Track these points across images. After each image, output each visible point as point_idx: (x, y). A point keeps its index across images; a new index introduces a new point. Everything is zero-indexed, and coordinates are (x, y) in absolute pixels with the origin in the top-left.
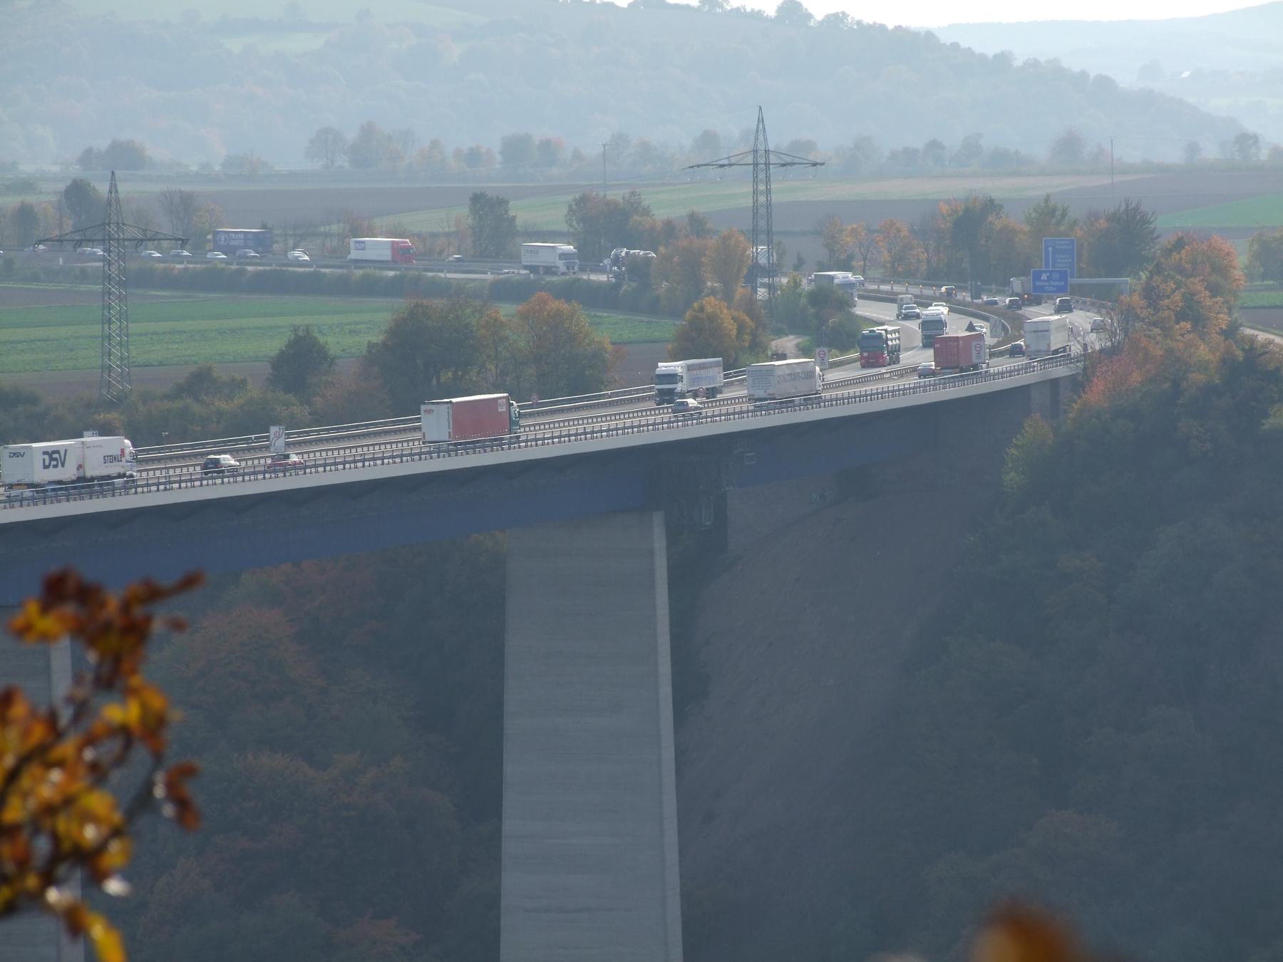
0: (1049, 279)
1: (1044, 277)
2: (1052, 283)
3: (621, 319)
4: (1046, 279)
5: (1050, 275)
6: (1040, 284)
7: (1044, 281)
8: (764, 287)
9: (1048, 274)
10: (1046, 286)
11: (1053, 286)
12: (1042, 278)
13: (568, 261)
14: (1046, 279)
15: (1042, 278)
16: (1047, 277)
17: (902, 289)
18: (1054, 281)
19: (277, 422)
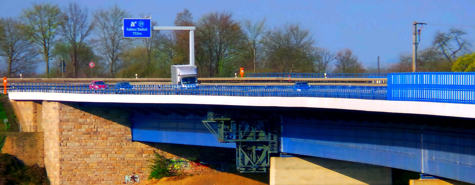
0: (137, 26)
1: (133, 24)
2: (139, 29)
3: (33, 143)
4: (134, 26)
5: (137, 23)
6: (130, 30)
7: (133, 27)
8: (78, 129)
9: (136, 22)
10: (134, 31)
11: (139, 32)
12: (131, 26)
13: (260, 166)
14: (134, 26)
15: (131, 26)
16: (135, 24)
17: (174, 158)
18: (141, 28)
19: (422, 134)
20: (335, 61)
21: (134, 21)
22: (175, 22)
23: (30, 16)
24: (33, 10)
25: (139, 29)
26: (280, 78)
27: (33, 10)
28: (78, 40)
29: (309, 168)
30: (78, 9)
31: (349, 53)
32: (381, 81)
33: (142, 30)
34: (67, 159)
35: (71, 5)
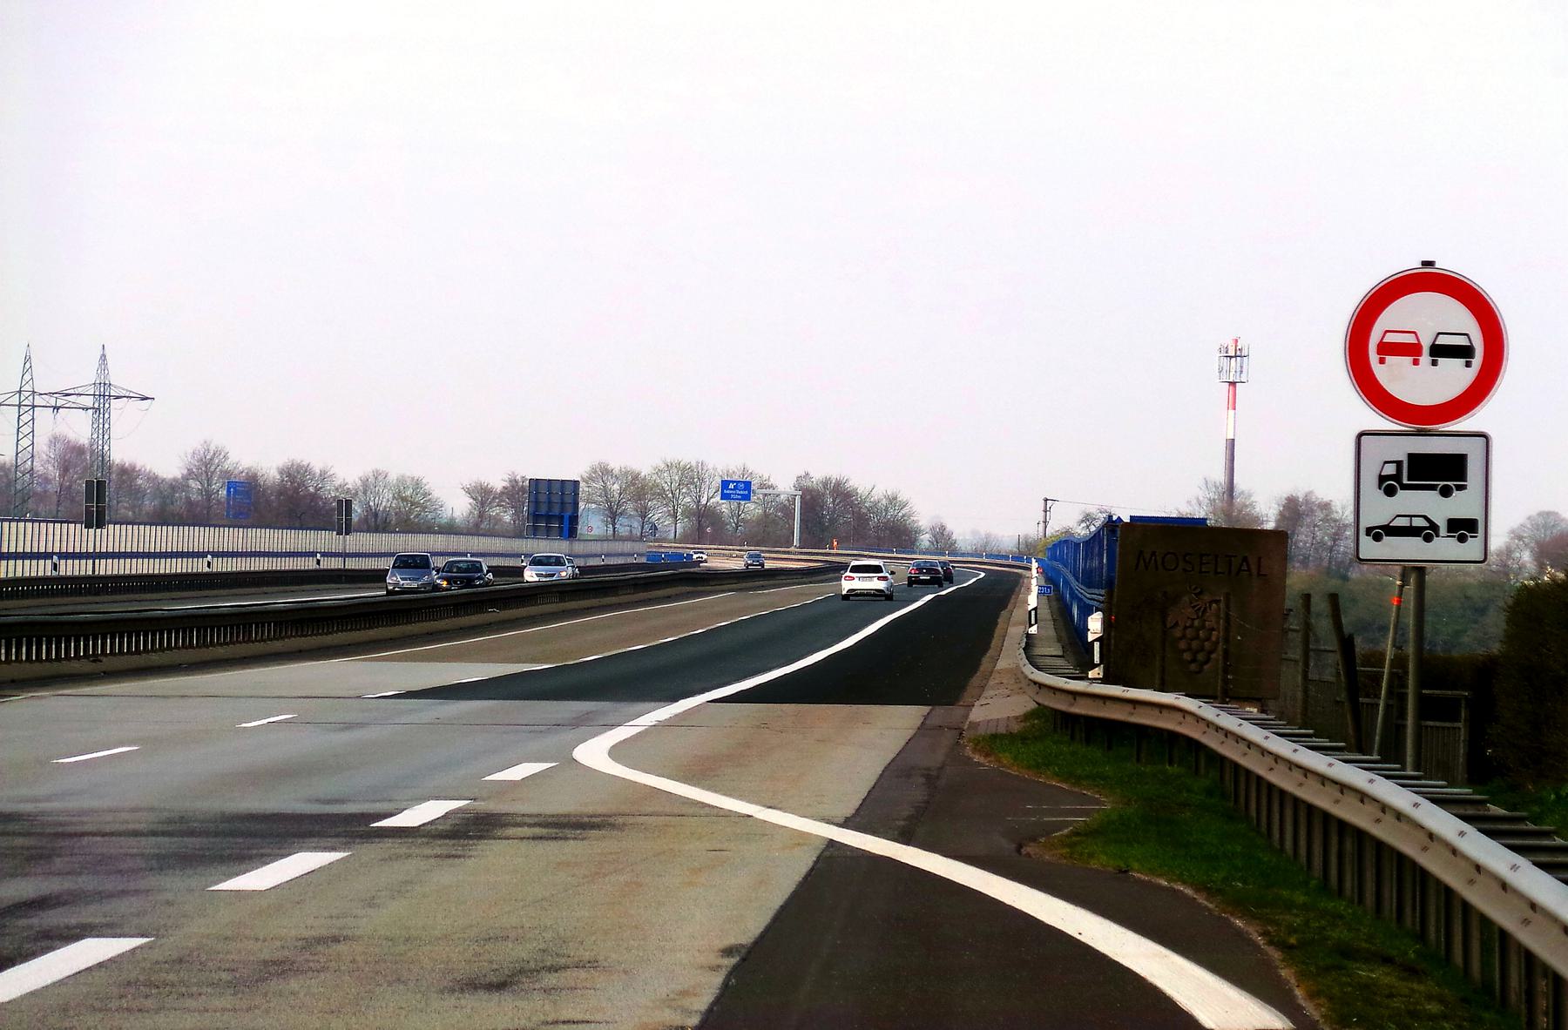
0: (736, 488)
1: (731, 486)
2: (738, 492)
6: (728, 492)
7: (731, 489)
20: (927, 536)
21: (733, 482)
22: (609, 468)
23: (659, 472)
24: (662, 466)
25: (738, 492)
26: (696, 546)
27: (662, 466)
28: (704, 501)
29: (398, 857)
30: (705, 468)
31: (943, 528)
32: (1201, 564)
33: (742, 492)
34: (261, 971)
35: (698, 463)
